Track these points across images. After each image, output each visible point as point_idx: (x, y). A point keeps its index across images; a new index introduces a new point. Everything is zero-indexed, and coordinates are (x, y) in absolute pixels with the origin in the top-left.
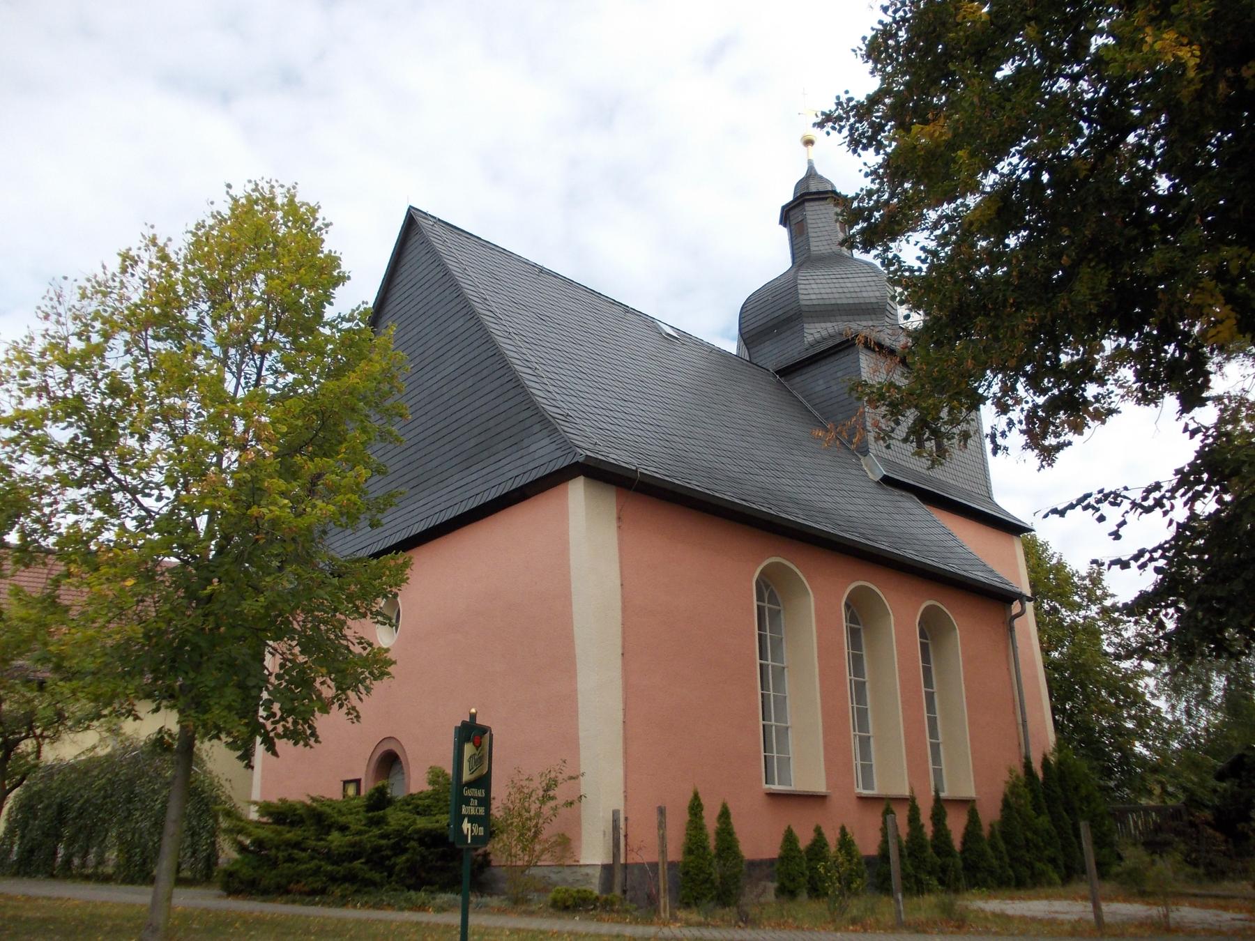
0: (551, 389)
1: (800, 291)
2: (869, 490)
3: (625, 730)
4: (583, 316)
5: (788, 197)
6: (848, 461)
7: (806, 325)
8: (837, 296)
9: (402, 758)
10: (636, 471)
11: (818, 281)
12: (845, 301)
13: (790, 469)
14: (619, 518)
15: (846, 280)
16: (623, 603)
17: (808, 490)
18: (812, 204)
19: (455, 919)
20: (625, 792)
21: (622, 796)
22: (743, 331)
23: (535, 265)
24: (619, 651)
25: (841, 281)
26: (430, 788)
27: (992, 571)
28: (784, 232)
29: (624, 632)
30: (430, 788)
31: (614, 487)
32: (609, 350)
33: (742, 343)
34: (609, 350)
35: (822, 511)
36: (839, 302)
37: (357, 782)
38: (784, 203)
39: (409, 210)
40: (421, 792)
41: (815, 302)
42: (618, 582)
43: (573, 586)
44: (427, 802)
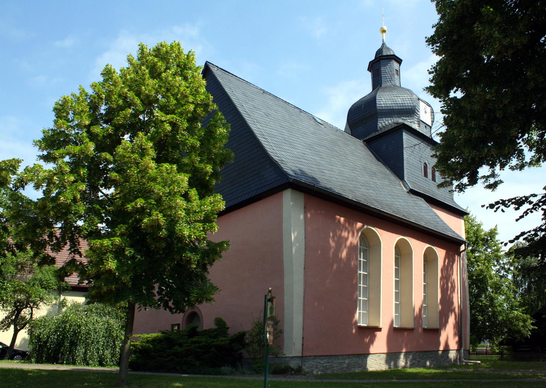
0: (275, 148)
1: (377, 103)
2: (404, 196)
3: (304, 300)
4: (283, 114)
5: (373, 58)
6: (396, 182)
7: (379, 119)
8: (394, 105)
9: (200, 315)
10: (314, 186)
11: (386, 98)
12: (397, 108)
13: (373, 186)
14: (305, 208)
15: (398, 98)
16: (305, 246)
17: (380, 195)
18: (384, 61)
19: (263, 379)
20: (303, 327)
21: (302, 328)
22: (349, 121)
23: (261, 89)
24: (303, 267)
25: (396, 98)
26: (216, 327)
27: (454, 232)
28: (369, 75)
29: (305, 259)
30: (216, 327)
31: (303, 194)
32: (296, 130)
33: (348, 127)
34: (296, 130)
35: (387, 205)
36: (394, 108)
37: (178, 325)
38: (371, 61)
39: (206, 63)
40: (210, 329)
41: (384, 108)
42: (304, 236)
43: (284, 239)
44: (215, 333)
